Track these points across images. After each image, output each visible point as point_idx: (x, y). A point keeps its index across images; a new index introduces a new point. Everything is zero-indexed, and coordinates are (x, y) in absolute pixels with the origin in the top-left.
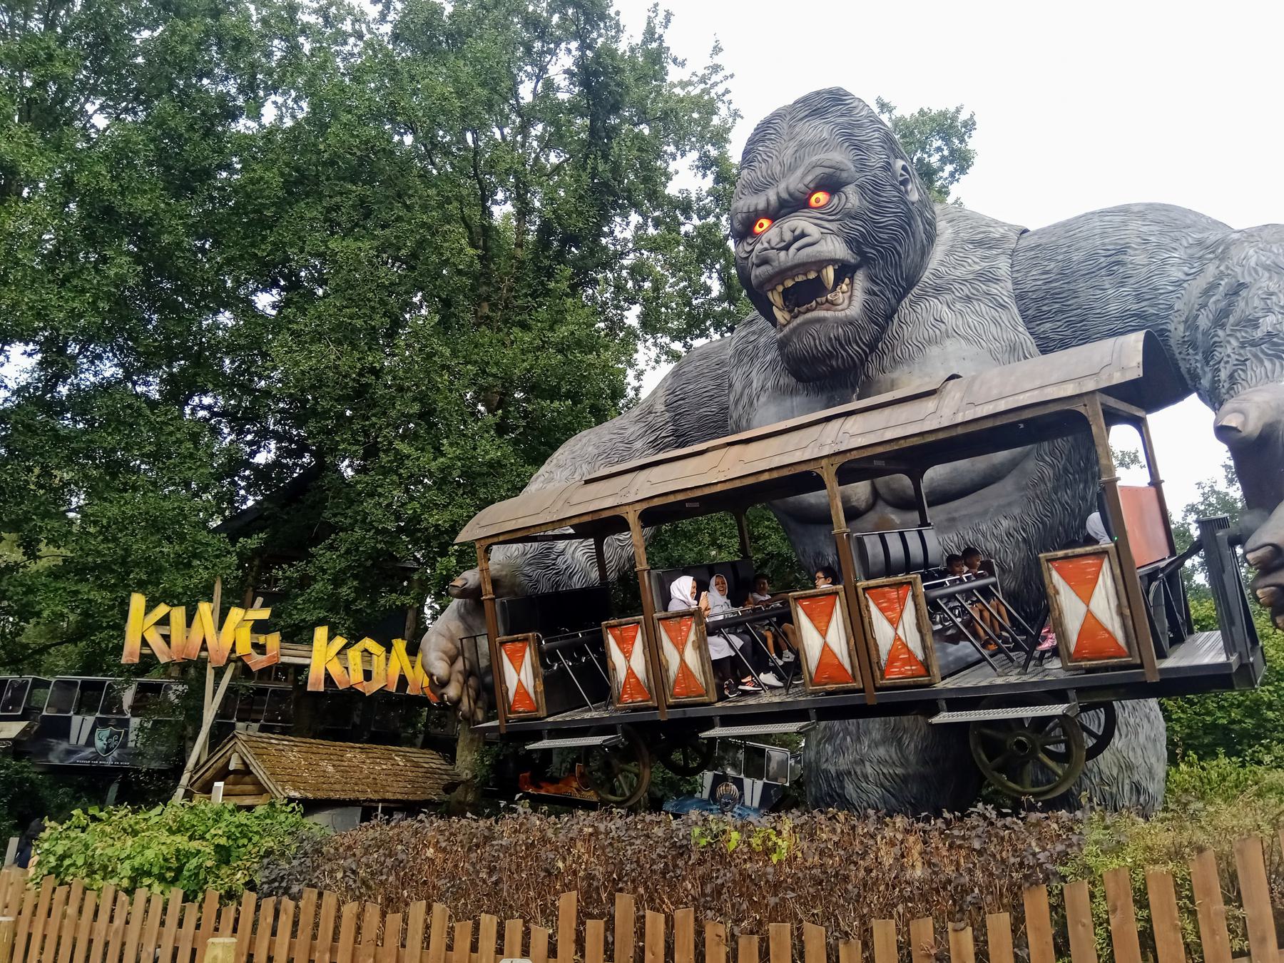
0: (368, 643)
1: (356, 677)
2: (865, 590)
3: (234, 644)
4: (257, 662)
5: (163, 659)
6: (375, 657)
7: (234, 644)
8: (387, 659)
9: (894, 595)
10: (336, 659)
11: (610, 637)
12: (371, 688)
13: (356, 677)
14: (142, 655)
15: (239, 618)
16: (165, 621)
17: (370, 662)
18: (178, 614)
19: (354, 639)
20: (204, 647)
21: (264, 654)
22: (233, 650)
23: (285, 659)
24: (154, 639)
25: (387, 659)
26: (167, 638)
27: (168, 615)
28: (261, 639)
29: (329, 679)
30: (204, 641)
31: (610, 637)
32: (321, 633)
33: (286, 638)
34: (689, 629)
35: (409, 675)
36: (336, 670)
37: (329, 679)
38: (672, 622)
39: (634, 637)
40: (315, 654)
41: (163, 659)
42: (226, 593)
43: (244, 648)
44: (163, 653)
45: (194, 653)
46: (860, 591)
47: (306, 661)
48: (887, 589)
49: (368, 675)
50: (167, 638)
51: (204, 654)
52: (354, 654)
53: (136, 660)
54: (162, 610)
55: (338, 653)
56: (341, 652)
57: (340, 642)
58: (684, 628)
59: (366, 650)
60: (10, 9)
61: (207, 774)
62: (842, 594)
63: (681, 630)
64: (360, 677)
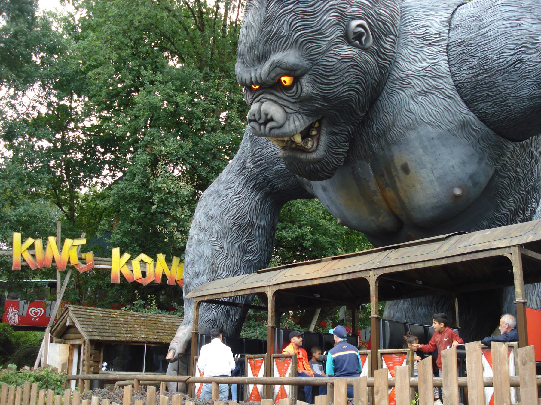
0: (143, 257)
1: (137, 275)
2: (382, 354)
3: (69, 259)
4: (82, 268)
5: (33, 268)
6: (148, 265)
7: (69, 259)
8: (155, 265)
9: (397, 360)
10: (125, 266)
11: (249, 364)
12: (146, 282)
13: (137, 275)
14: (22, 266)
15: (70, 245)
16: (32, 247)
17: (145, 267)
18: (38, 243)
19: (134, 254)
20: (54, 261)
21: (85, 264)
22: (69, 262)
23: (98, 266)
24: (27, 256)
25: (155, 265)
26: (34, 256)
27: (33, 243)
28: (83, 256)
29: (122, 275)
30: (53, 258)
31: (249, 364)
32: (116, 251)
33: (96, 255)
34: (288, 365)
35: (167, 273)
36: (126, 271)
37: (122, 275)
38: (280, 360)
39: (260, 366)
40: (113, 263)
41: (33, 268)
42: (63, 231)
43: (74, 260)
44: (33, 264)
45: (49, 265)
46: (379, 355)
47: (108, 267)
48: (393, 356)
49: (144, 274)
50: (34, 256)
51: (54, 264)
52: (136, 263)
53: (20, 268)
54: (30, 241)
55: (127, 263)
56: (129, 263)
57: (127, 256)
58: (286, 365)
59: (142, 261)
60: (5, 350)
61: (58, 328)
62: (369, 355)
63: (284, 366)
64: (140, 275)
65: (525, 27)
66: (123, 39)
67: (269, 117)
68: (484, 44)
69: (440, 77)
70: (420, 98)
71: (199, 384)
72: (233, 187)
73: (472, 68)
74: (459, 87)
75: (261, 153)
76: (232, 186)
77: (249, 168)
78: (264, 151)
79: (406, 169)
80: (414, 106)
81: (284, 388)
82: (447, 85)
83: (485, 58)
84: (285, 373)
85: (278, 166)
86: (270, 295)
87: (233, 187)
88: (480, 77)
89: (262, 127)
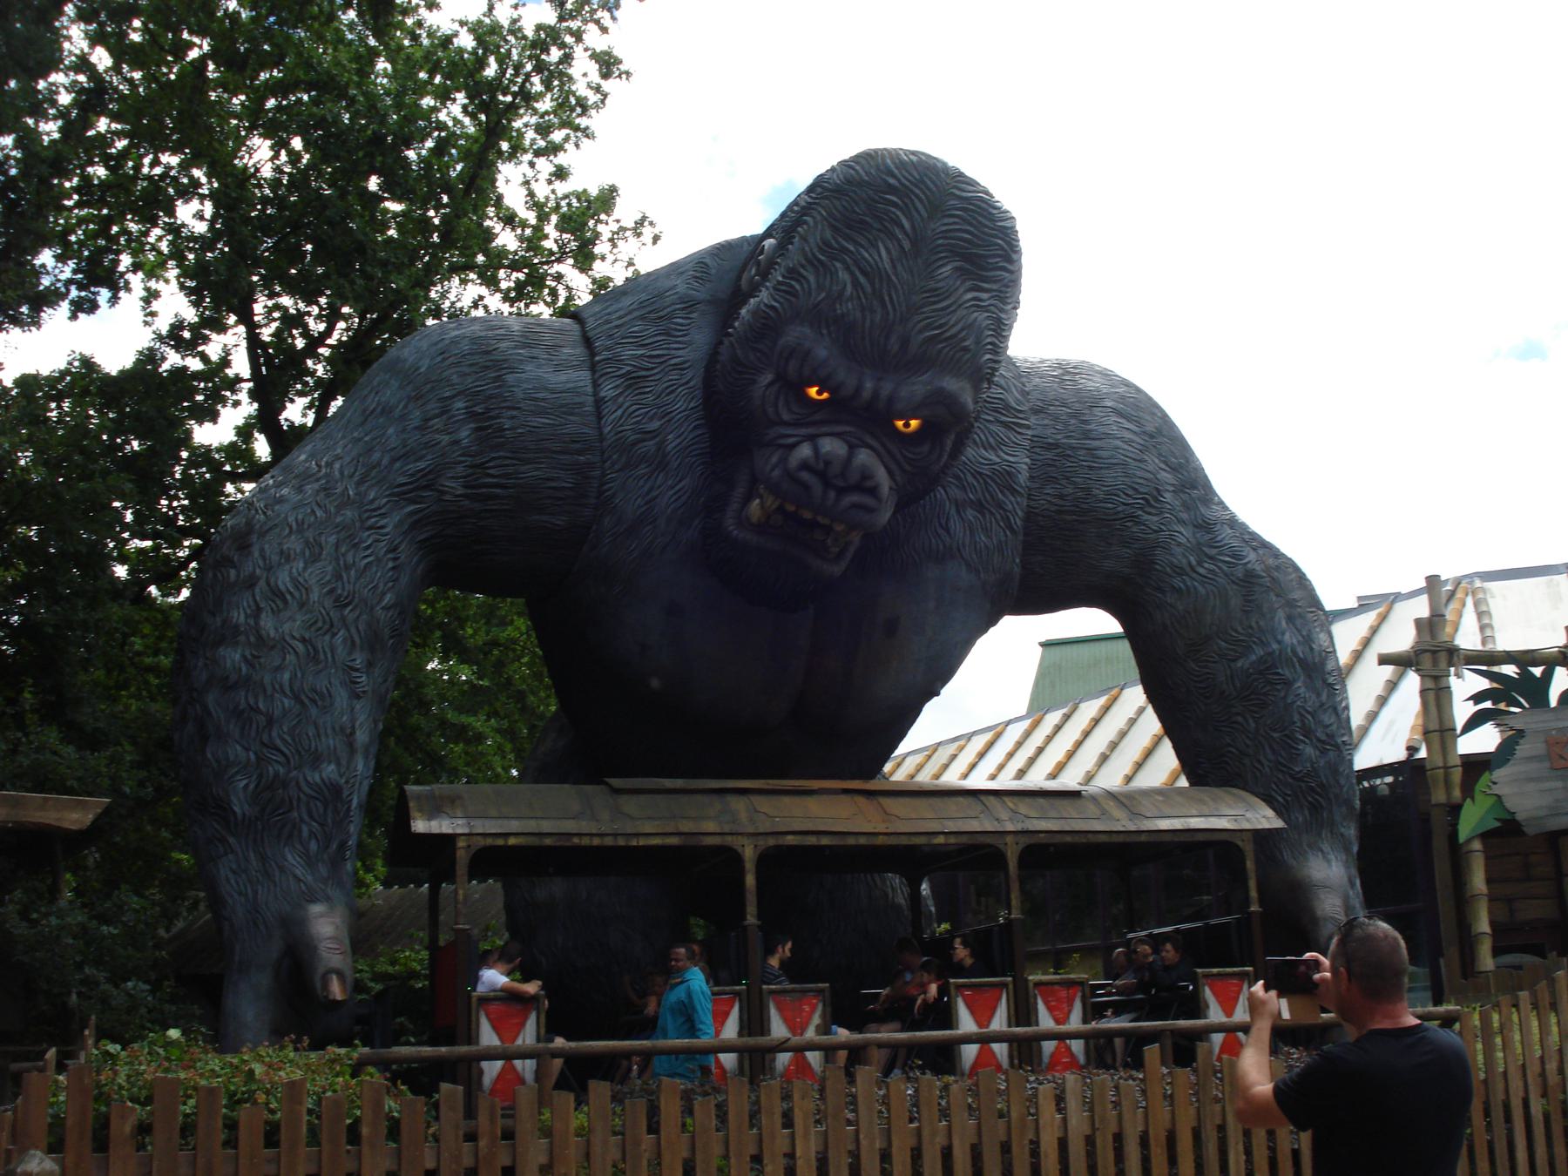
2: (1038, 984)
9: (1064, 994)
58: (807, 1008)
65: (1150, 468)
66: (460, 116)
67: (869, 484)
68: (1090, 468)
69: (1014, 492)
70: (970, 513)
71: (499, 1064)
72: (382, 527)
73: (1061, 497)
74: (1029, 516)
75: (510, 470)
76: (382, 523)
77: (443, 493)
78: (523, 468)
79: (891, 628)
80: (956, 525)
81: (804, 1058)
82: (1017, 507)
83: (1088, 490)
84: (803, 1029)
85: (544, 518)
86: (749, 853)
87: (382, 527)
88: (1069, 518)
89: (832, 494)
